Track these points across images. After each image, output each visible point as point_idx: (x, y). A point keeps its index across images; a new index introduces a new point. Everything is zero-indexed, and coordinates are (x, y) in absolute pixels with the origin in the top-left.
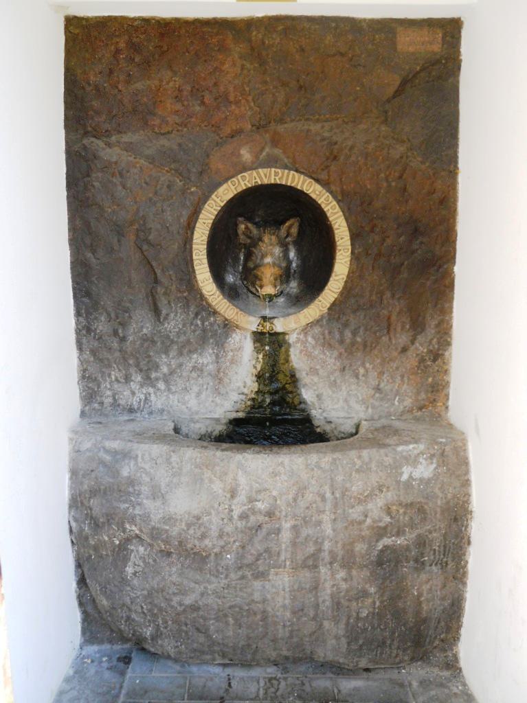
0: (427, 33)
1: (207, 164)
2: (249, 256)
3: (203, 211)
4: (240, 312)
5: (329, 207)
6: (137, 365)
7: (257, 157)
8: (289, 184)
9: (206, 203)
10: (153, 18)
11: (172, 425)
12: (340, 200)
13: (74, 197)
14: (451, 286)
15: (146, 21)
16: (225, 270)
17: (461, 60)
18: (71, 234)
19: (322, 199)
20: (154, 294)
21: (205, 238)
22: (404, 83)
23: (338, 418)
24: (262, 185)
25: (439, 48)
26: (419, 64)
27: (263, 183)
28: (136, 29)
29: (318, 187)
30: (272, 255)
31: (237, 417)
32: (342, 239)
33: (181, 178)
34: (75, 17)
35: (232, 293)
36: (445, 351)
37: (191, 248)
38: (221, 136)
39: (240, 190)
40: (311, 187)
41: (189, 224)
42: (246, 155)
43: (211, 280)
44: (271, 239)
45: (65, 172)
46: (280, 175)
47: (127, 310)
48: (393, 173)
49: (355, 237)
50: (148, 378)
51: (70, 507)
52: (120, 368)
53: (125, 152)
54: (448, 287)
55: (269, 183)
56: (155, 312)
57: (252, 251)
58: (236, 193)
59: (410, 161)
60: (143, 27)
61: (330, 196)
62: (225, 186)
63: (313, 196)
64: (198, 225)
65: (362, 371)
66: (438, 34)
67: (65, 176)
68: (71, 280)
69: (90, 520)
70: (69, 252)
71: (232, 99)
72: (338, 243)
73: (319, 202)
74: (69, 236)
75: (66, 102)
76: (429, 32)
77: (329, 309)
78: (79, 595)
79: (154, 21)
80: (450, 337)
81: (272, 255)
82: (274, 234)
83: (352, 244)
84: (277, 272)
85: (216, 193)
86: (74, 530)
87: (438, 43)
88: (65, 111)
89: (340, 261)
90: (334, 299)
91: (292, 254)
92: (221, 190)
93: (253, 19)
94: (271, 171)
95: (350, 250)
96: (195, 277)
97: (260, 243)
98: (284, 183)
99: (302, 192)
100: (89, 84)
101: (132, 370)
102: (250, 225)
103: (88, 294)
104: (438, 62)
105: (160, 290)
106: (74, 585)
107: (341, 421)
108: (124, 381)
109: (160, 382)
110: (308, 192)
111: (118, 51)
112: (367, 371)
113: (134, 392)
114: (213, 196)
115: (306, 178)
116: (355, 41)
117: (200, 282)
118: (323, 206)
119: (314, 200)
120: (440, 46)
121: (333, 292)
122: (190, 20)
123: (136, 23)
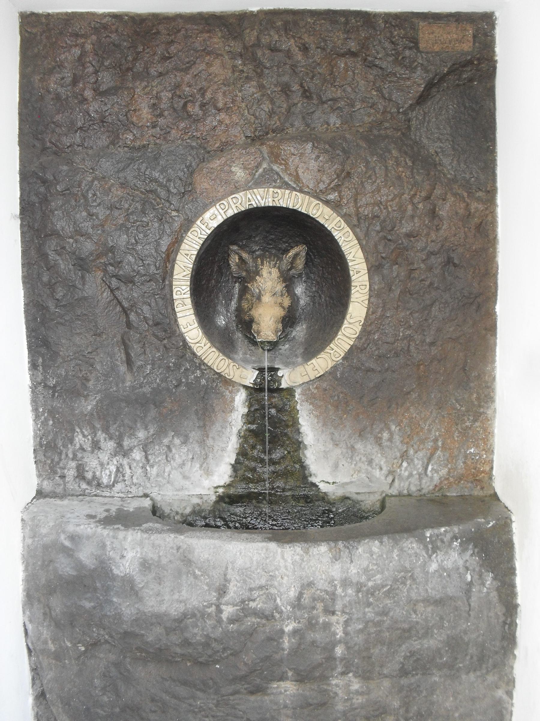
0: (454, 30)
2: (244, 290)
3: (185, 241)
4: (232, 364)
9: (189, 230)
10: (127, 14)
12: (355, 226)
13: (29, 226)
14: (492, 329)
15: (117, 17)
16: (216, 312)
17: (496, 61)
18: (25, 269)
20: (127, 341)
21: (188, 272)
22: (430, 85)
23: (357, 493)
24: (257, 208)
25: (470, 47)
26: (447, 66)
28: (105, 27)
29: (327, 211)
30: (269, 296)
32: (358, 272)
34: (33, 14)
35: (224, 342)
36: (488, 408)
37: (171, 286)
38: (208, 149)
40: (318, 210)
41: (168, 256)
42: (239, 174)
43: (196, 325)
45: (19, 196)
46: (197, 230)
48: (418, 193)
49: (374, 269)
50: (120, 445)
52: (86, 433)
54: (490, 330)
56: (128, 364)
57: (247, 287)
58: (225, 218)
60: (113, 25)
61: (342, 221)
62: (213, 210)
63: (322, 221)
64: (179, 257)
65: (386, 435)
66: (468, 31)
67: (19, 201)
68: (24, 326)
69: (50, 621)
70: (22, 293)
71: (220, 105)
72: (353, 278)
73: (329, 229)
74: (23, 272)
75: (20, 114)
76: (457, 28)
77: (344, 358)
78: (37, 713)
79: (126, 18)
80: (493, 390)
81: (269, 296)
85: (201, 218)
87: (468, 41)
88: (19, 124)
89: (352, 244)
90: (349, 347)
91: (299, 290)
92: (207, 215)
93: (246, 13)
95: (368, 287)
96: (176, 321)
99: (308, 216)
100: (49, 92)
101: (101, 436)
102: (245, 255)
103: (46, 343)
104: (470, 63)
105: (134, 336)
106: (30, 700)
107: (359, 498)
108: (89, 449)
109: (135, 451)
111: (83, 54)
112: (391, 434)
113: (103, 464)
114: (198, 222)
115: (312, 199)
116: (369, 39)
119: (323, 226)
120: (471, 44)
121: (347, 337)
122: (171, 15)
123: (104, 21)
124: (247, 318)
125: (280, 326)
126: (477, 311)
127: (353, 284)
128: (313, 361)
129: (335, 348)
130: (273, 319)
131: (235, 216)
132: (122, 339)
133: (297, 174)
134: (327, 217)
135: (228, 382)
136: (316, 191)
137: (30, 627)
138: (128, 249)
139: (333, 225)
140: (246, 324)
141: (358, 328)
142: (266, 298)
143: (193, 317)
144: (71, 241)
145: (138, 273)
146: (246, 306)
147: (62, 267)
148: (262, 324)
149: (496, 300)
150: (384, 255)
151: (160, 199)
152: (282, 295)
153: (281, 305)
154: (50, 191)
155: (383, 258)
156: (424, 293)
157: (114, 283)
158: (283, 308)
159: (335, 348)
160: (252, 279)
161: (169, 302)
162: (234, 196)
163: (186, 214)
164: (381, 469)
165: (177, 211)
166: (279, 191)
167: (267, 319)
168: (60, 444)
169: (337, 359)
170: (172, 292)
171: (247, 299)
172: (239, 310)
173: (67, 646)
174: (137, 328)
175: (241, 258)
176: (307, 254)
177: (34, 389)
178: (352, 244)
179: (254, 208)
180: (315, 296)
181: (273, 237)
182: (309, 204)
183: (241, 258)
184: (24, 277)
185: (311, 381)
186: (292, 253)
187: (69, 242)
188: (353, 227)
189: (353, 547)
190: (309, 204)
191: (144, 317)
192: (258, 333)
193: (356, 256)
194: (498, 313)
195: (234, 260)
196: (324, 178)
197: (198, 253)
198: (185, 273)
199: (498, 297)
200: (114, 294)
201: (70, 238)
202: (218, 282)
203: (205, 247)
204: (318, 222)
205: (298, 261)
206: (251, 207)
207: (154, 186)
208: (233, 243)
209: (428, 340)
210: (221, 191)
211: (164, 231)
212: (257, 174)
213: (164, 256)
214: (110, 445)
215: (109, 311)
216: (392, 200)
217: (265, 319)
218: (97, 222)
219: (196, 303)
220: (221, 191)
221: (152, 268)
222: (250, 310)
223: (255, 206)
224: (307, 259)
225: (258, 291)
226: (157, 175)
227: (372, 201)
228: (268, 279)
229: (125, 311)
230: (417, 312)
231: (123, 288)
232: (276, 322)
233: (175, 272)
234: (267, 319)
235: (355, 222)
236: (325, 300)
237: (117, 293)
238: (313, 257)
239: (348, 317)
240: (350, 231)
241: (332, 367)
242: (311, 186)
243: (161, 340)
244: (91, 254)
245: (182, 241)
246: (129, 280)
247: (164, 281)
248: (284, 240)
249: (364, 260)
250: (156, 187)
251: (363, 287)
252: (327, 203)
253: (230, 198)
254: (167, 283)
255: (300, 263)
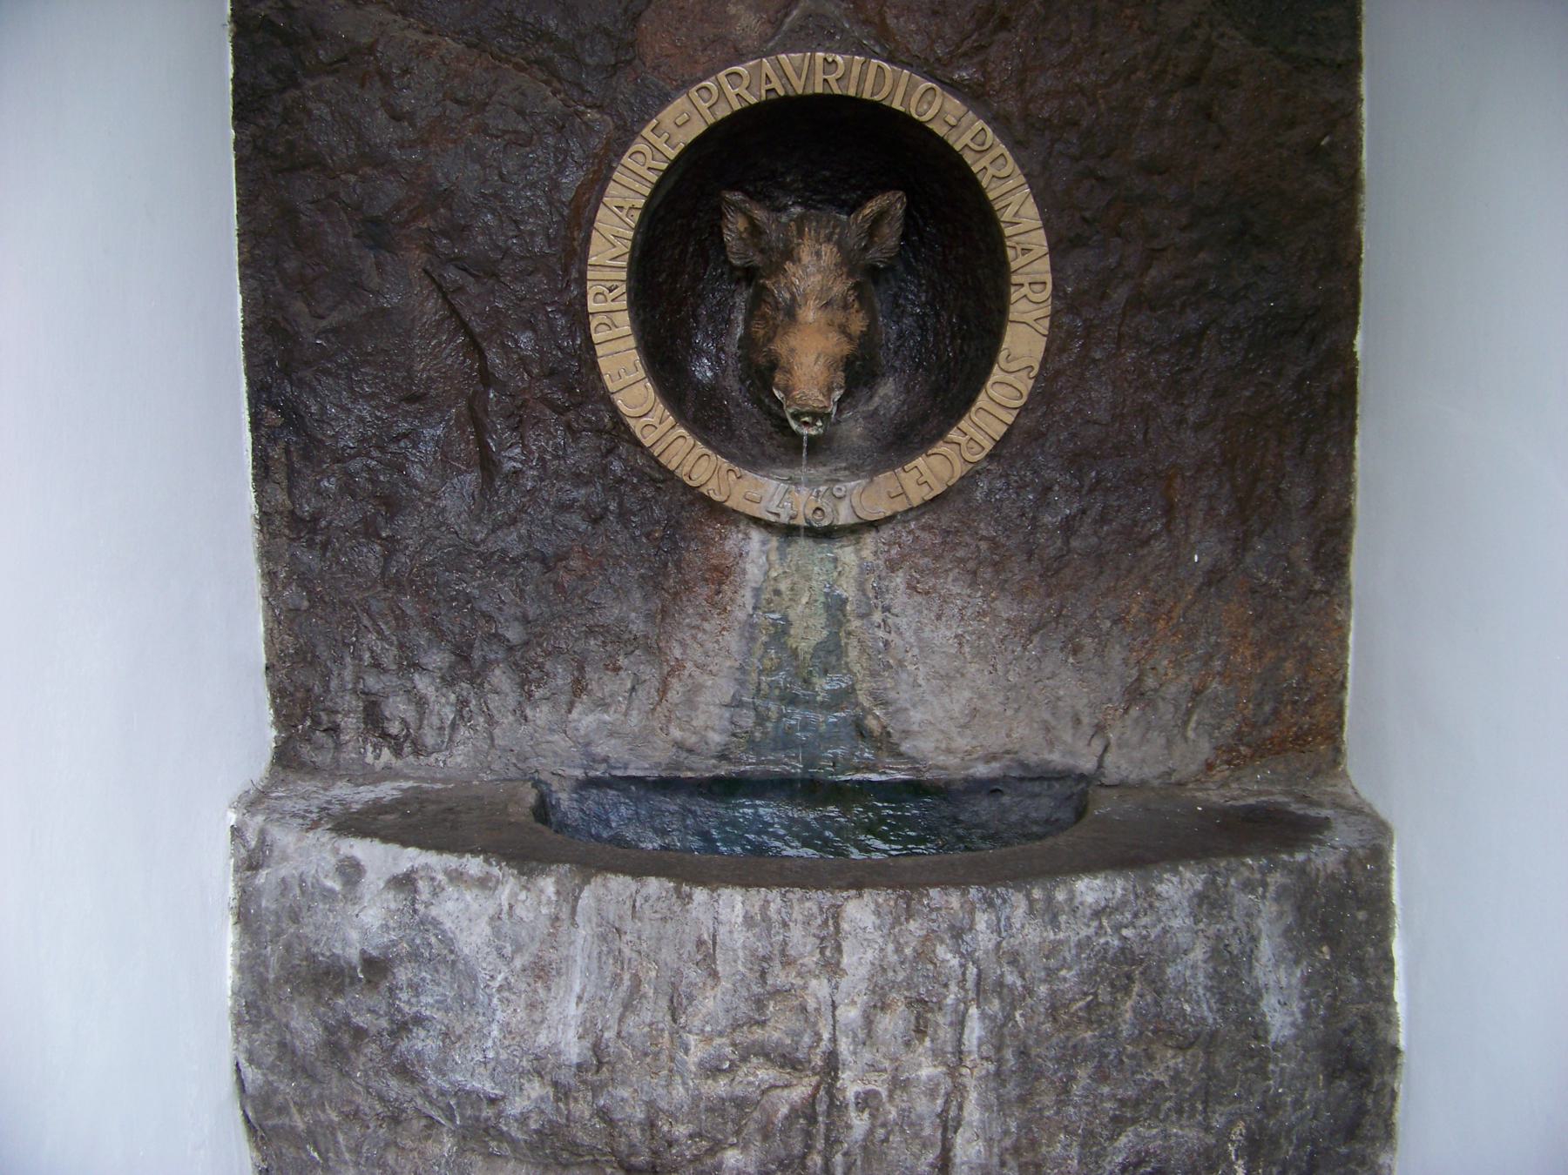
1: (632, 45)
2: (760, 297)
5: (984, 162)
6: (432, 624)
7: (776, 24)
8: (866, 96)
11: (531, 797)
13: (255, 147)
19: (966, 139)
27: (791, 93)
29: (954, 106)
31: (1393, 913)
32: (1026, 251)
33: (556, 84)
39: (723, 112)
40: (930, 104)
43: (642, 373)
44: (818, 254)
47: (549, 934)
48: (1170, 68)
49: (1059, 248)
51: (239, 1021)
53: (399, 18)
55: (809, 91)
56: (483, 468)
57: (764, 287)
58: (711, 120)
59: (1222, 36)
61: (989, 131)
62: (680, 103)
63: (939, 129)
64: (602, 213)
73: (957, 147)
82: (829, 239)
83: (1054, 269)
84: (837, 350)
86: (249, 1088)
90: (1005, 429)
92: (668, 115)
94: (812, 58)
95: (1049, 286)
97: (788, 265)
98: (852, 92)
99: (905, 119)
102: (760, 214)
103: (294, 418)
109: (497, 672)
110: (923, 119)
114: (646, 132)
117: (606, 377)
118: (969, 158)
119: (942, 142)
124: (762, 361)
125: (840, 377)
126: (1308, 350)
127: (1015, 279)
128: (920, 461)
129: (972, 431)
130: (822, 360)
131: (736, 116)
132: (470, 408)
133: (883, 20)
134: (953, 121)
135: (719, 512)
136: (926, 60)
137: (250, 1073)
138: (483, 195)
139: (966, 139)
140: (762, 372)
141: (1025, 385)
142: (810, 314)
143: (635, 356)
144: (352, 178)
145: (506, 252)
146: (762, 332)
147: (331, 239)
148: (798, 372)
149: (1355, 323)
150: (1087, 214)
151: (560, 80)
152: (846, 307)
153: (843, 330)
154: (303, 63)
155: (1084, 219)
156: (1183, 306)
157: (452, 274)
158: (850, 337)
159: (972, 431)
160: (777, 269)
161: (579, 317)
162: (729, 70)
163: (620, 116)
164: (1077, 721)
165: (599, 108)
166: (838, 58)
167: (810, 359)
168: (323, 651)
169: (978, 457)
170: (584, 295)
171: (763, 317)
172: (748, 341)
173: (332, 1121)
174: (505, 385)
175: (751, 221)
176: (908, 213)
177: (265, 519)
178: (1011, 183)
179: (781, 99)
180: (925, 314)
181: (827, 174)
182: (911, 87)
183: (751, 221)
184: (243, 264)
185: (911, 509)
186: (871, 208)
187: (346, 183)
188: (1017, 146)
189: (1005, 901)
190: (911, 87)
191: (521, 358)
192: (787, 391)
193: (1022, 212)
194: (1359, 356)
195: (734, 228)
196: (948, 31)
197: (647, 205)
198: (615, 252)
199: (1361, 318)
200: (451, 304)
201: (349, 172)
202: (697, 279)
203: (663, 192)
204: (932, 133)
205: (886, 230)
206: (772, 96)
207: (542, 50)
208: (733, 187)
209: (1191, 418)
210: (703, 60)
211: (566, 152)
212: (789, 20)
213: (566, 212)
214: (438, 659)
215: (440, 343)
216: (1107, 85)
217: (804, 360)
218: (411, 135)
219: (643, 322)
220: (703, 60)
221: (539, 240)
222: (770, 340)
223: (782, 93)
224: (906, 225)
225: (788, 296)
226: (552, 23)
227: (1061, 88)
228: (813, 272)
229: (475, 347)
230: (1166, 350)
231: (473, 288)
232: (831, 366)
233: (593, 250)
234: (810, 359)
235: (1018, 133)
236: (950, 322)
237: (458, 301)
238: (921, 222)
239: (1003, 355)
240: (1007, 154)
241: (962, 478)
242: (914, 48)
243: (560, 410)
244: (398, 208)
245: (608, 179)
246: (485, 270)
247: (566, 271)
248: (853, 181)
249: (1040, 224)
250: (550, 53)
251: (1037, 288)
252: (953, 88)
253: (721, 75)
254: (574, 275)
255: (890, 236)
